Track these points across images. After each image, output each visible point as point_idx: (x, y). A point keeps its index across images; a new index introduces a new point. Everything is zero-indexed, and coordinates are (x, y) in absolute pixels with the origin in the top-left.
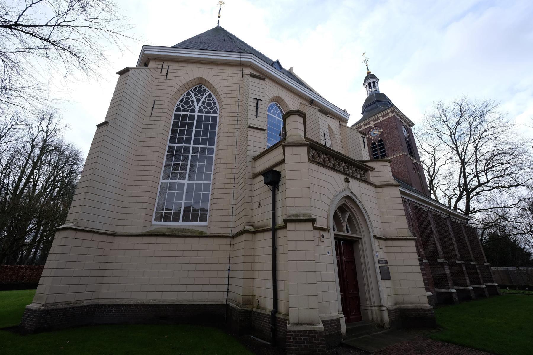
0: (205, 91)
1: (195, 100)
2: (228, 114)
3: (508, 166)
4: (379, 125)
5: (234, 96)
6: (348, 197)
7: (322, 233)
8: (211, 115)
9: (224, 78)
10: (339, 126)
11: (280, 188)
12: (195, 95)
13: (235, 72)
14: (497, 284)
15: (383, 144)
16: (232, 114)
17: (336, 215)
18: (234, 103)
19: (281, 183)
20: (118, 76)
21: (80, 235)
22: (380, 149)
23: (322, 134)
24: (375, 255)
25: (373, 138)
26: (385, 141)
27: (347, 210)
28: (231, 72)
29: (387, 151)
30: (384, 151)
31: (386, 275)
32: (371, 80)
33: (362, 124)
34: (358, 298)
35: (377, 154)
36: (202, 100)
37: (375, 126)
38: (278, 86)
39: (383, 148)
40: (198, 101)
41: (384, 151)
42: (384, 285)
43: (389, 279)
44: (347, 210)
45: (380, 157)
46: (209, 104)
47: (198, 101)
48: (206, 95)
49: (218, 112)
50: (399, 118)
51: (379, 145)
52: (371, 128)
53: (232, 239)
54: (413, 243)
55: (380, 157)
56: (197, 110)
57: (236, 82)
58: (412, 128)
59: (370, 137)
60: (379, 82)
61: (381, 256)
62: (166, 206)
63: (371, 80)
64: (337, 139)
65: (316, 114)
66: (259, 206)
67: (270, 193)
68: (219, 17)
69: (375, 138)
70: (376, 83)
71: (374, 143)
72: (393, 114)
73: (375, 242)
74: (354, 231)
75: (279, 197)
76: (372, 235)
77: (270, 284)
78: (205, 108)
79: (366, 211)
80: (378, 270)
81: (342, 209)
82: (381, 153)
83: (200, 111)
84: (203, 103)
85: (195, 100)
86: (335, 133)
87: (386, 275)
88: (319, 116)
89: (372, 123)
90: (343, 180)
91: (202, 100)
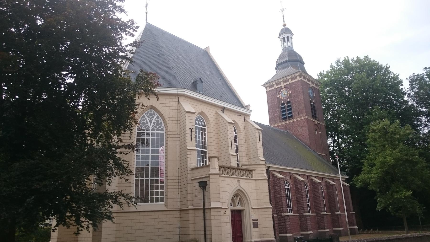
1: (148, 121)
2: (171, 133)
4: (288, 86)
5: (174, 119)
6: (239, 190)
7: (225, 210)
8: (160, 132)
9: (167, 105)
10: (243, 120)
11: (207, 189)
12: (149, 117)
13: (174, 100)
14: (356, 227)
15: (290, 106)
16: (174, 133)
17: (233, 199)
18: (174, 125)
19: (207, 187)
22: (288, 110)
23: (230, 140)
24: (251, 216)
25: (282, 99)
26: (293, 103)
27: (239, 196)
28: (171, 100)
29: (293, 114)
30: (291, 113)
31: (256, 225)
32: (286, 34)
33: (274, 83)
35: (285, 115)
36: (153, 121)
37: (285, 86)
38: (201, 103)
39: (291, 109)
40: (151, 121)
41: (291, 113)
42: (255, 231)
43: (258, 227)
44: (239, 196)
45: (287, 118)
47: (151, 121)
49: (164, 129)
50: (306, 81)
51: (288, 107)
54: (271, 210)
55: (287, 118)
56: (151, 129)
57: (174, 108)
59: (281, 97)
60: (293, 37)
61: (255, 217)
63: (286, 34)
64: (242, 131)
65: (225, 125)
66: (196, 196)
67: (202, 191)
68: (146, 13)
69: (285, 99)
70: (290, 38)
71: (283, 104)
72: (301, 79)
73: (251, 210)
74: (242, 206)
75: (206, 193)
76: (250, 207)
77: (203, 233)
78: (156, 127)
79: (248, 196)
80: (252, 224)
81: (236, 195)
82: (289, 114)
83: (153, 130)
84: (154, 123)
85: (148, 121)
86: (241, 127)
87: (256, 225)
88: (228, 126)
89: (282, 83)
90: (237, 181)
91: (153, 121)
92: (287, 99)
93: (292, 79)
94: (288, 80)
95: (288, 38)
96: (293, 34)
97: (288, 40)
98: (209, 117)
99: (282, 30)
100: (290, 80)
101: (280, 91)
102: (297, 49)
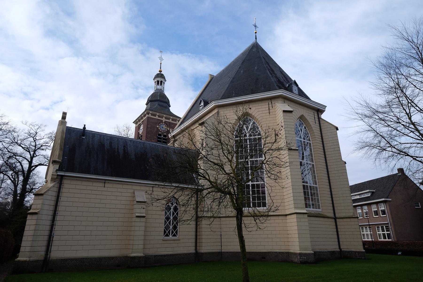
0: (250, 120)
3: (390, 123)
20: (82, 128)
21: (228, 219)
34: (86, 258)
36: (250, 127)
37: (165, 122)
40: (247, 128)
46: (254, 128)
48: (251, 123)
52: (162, 121)
53: (258, 230)
58: (379, 100)
60: (166, 83)
62: (301, 208)
83: (250, 135)
89: (164, 118)
91: (250, 127)
92: (165, 133)
93: (173, 120)
94: (169, 119)
95: (161, 82)
96: (164, 78)
97: (161, 84)
98: (309, 121)
99: (158, 74)
100: (171, 120)
101: (160, 123)
102: (167, 93)
